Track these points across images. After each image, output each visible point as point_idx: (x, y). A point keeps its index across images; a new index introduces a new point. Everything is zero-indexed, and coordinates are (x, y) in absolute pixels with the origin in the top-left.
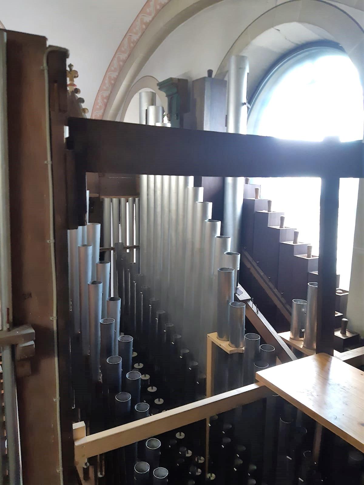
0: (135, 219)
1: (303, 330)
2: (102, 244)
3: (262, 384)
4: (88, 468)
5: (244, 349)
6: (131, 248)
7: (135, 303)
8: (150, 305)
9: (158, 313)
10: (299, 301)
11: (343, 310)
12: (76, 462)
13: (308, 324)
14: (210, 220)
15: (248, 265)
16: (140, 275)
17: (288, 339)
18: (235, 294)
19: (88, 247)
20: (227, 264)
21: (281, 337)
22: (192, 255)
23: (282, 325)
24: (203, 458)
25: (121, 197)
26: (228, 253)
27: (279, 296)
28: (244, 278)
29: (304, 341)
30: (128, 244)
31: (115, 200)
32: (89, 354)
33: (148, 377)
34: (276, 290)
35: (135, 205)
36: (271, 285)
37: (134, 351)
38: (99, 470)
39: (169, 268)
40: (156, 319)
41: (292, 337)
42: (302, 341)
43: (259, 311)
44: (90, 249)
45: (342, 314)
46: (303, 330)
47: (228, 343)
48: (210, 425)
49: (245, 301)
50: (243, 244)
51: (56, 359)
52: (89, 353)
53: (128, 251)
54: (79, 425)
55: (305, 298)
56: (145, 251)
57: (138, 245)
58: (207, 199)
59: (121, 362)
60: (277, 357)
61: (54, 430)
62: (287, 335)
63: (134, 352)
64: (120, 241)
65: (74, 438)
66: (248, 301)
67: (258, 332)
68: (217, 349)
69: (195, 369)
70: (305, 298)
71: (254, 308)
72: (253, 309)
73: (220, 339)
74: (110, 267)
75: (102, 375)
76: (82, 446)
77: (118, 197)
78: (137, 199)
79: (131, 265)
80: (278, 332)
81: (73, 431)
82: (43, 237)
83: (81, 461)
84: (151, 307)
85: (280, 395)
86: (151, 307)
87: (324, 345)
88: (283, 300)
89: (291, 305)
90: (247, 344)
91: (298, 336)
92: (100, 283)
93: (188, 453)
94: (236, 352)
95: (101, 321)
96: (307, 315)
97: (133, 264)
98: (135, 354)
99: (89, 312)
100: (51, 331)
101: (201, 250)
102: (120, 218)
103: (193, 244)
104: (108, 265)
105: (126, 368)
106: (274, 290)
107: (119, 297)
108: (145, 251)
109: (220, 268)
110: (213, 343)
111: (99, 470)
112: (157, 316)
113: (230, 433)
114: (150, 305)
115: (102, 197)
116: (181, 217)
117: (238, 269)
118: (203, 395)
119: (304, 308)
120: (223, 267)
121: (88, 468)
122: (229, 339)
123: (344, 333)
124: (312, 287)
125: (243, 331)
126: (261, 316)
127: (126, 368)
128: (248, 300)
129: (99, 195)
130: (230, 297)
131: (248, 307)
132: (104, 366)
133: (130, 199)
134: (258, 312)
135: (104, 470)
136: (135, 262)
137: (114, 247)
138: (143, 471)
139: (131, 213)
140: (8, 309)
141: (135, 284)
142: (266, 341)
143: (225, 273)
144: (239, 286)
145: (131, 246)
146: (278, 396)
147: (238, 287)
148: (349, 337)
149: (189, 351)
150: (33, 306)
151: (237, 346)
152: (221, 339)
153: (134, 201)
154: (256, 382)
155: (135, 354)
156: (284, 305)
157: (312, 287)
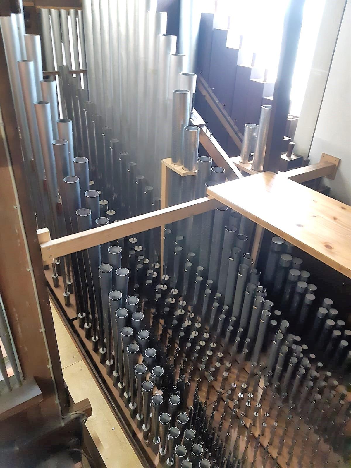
0: (80, 37)
1: (252, 154)
2: (44, 67)
4: (57, 278)
5: (196, 171)
6: (78, 72)
8: (103, 134)
10: (251, 125)
11: (291, 135)
12: (44, 262)
13: (257, 148)
14: (164, 35)
15: (204, 93)
16: (90, 102)
17: (238, 163)
18: (189, 119)
19: (29, 62)
20: (182, 86)
22: (146, 77)
23: (233, 151)
24: (156, 273)
25: (60, 8)
26: (184, 74)
27: (232, 123)
28: (199, 103)
29: (252, 164)
30: (74, 68)
31: (54, 12)
32: (46, 179)
33: (106, 202)
34: (230, 118)
35: (78, 20)
36: (225, 112)
37: (90, 180)
38: (67, 278)
40: (110, 147)
41: (242, 161)
42: (250, 164)
43: (212, 136)
44: (31, 64)
45: (290, 139)
46: (252, 154)
48: (164, 238)
49: (200, 126)
50: (200, 65)
51: (10, 168)
52: (45, 178)
54: (43, 231)
55: (257, 122)
56: (288, 297)
57: (84, 69)
58: (160, 9)
60: (226, 178)
61: (19, 236)
62: (238, 159)
63: (91, 181)
64: (65, 64)
66: (202, 126)
67: (209, 156)
68: (171, 173)
69: (150, 193)
70: (257, 122)
71: (208, 133)
72: (206, 134)
73: (174, 163)
74: (55, 85)
75: (60, 198)
76: (48, 248)
77: (58, 7)
78: (79, 11)
79: (79, 91)
80: (230, 156)
81: (38, 235)
83: (49, 259)
84: (104, 136)
86: (104, 136)
87: (272, 164)
88: (235, 127)
89: (242, 131)
91: (247, 161)
92: (47, 103)
93: (145, 261)
95: (53, 142)
96: (257, 139)
97: (81, 90)
98: (92, 183)
99: (40, 133)
101: (155, 72)
102: (62, 36)
103: (146, 64)
104: (53, 84)
106: (228, 118)
107: (69, 118)
108: (94, 76)
109: (175, 90)
111: (67, 278)
113: (182, 243)
114: (103, 134)
115: (39, 7)
116: (131, 32)
117: (194, 92)
118: (158, 207)
119: (256, 133)
121: (57, 278)
122: (182, 163)
123: (289, 156)
124: (266, 109)
125: (197, 155)
126: (214, 140)
128: (203, 125)
129: (34, 4)
131: (201, 131)
132: (62, 185)
133: (72, 11)
134: (211, 137)
135: (71, 277)
136: (83, 88)
137: (59, 71)
139: (74, 26)
141: (86, 112)
143: (180, 95)
144: (194, 111)
145: (77, 70)
148: (294, 159)
149: (144, 177)
151: (190, 169)
154: (207, 196)
155: (92, 183)
156: (236, 134)
157: (266, 109)
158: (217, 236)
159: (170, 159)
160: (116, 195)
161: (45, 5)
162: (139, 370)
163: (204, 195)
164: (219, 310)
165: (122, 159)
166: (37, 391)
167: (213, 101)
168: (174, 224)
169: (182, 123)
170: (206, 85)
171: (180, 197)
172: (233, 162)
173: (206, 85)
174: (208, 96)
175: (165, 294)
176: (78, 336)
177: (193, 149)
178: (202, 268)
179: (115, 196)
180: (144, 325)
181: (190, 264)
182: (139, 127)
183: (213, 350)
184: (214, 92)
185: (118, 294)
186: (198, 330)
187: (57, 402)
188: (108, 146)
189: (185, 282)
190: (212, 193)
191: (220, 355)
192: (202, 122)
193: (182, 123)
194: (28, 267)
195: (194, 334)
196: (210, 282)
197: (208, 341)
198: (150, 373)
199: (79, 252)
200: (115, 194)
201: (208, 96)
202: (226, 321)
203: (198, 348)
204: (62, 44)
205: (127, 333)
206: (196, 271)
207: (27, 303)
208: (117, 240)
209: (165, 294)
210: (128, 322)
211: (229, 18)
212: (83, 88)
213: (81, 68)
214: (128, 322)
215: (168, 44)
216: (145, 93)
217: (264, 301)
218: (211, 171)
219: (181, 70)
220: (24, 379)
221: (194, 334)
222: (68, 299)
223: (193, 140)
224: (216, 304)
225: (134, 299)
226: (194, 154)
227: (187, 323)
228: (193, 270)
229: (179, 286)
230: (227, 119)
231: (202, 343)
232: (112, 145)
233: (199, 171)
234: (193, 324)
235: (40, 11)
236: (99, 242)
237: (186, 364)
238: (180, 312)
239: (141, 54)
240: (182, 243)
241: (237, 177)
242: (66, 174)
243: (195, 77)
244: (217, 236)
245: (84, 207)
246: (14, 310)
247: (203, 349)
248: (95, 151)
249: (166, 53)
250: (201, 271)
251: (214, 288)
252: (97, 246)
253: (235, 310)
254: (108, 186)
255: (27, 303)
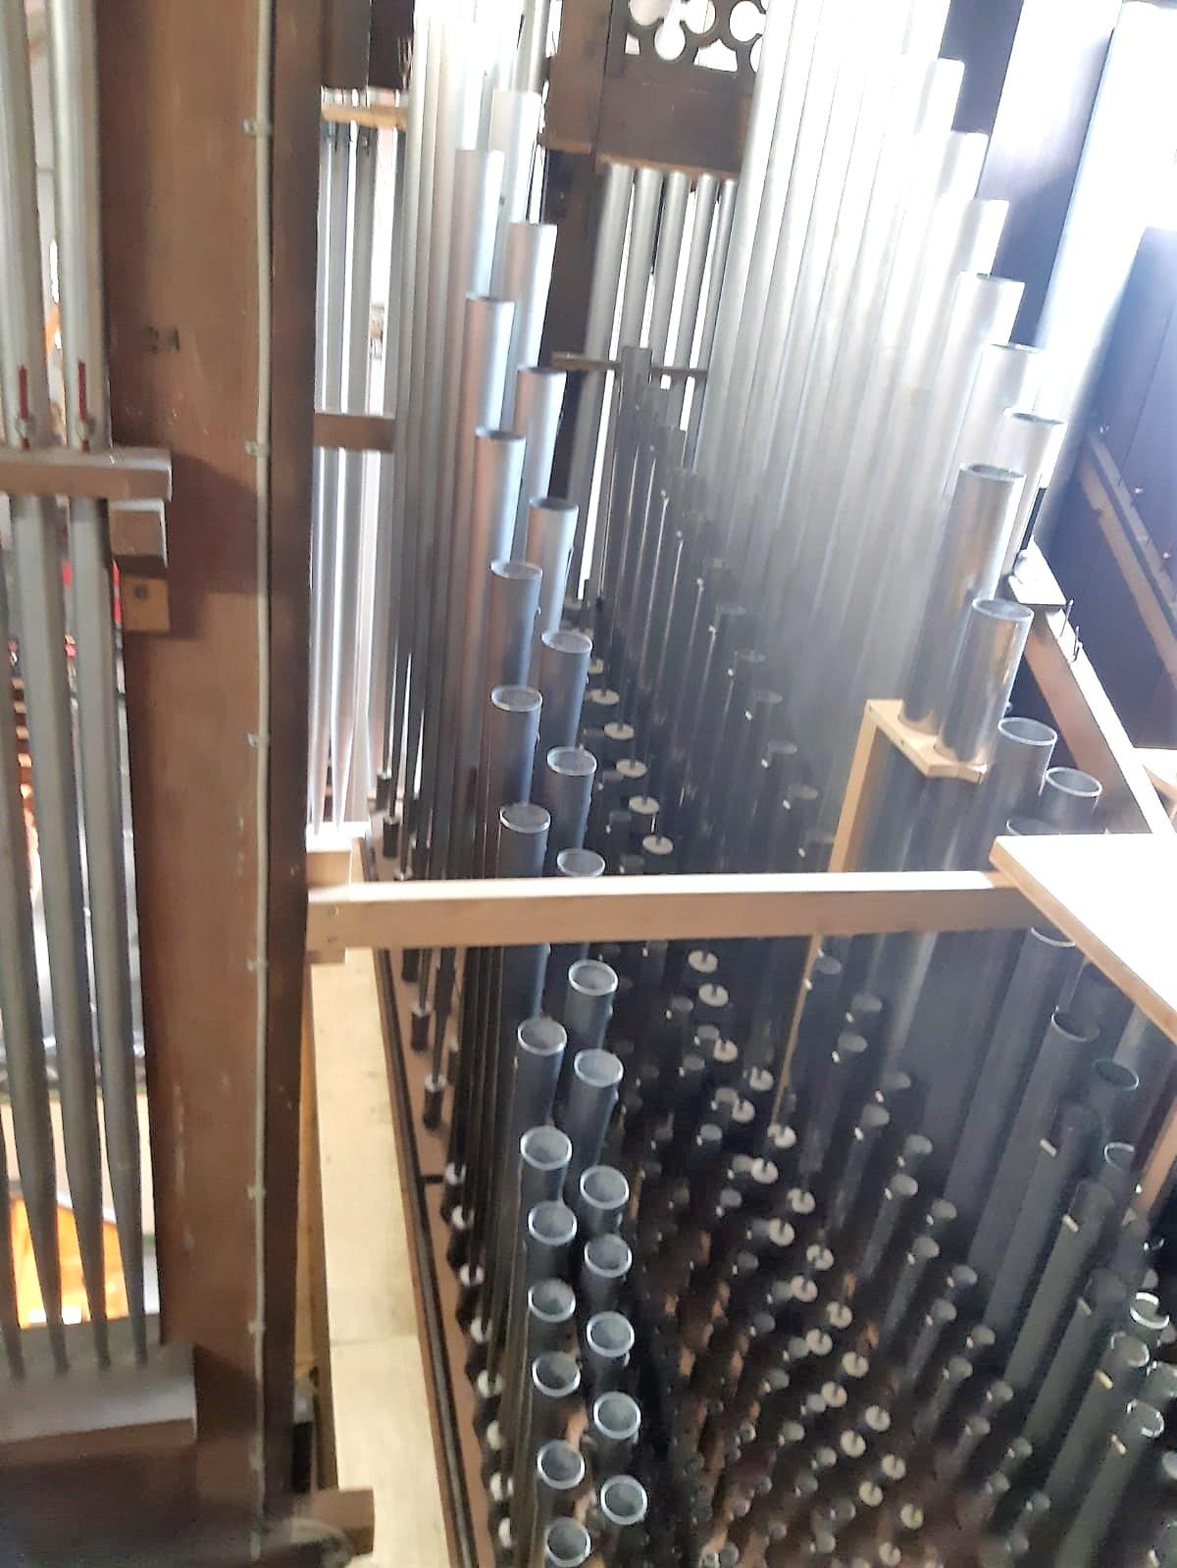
3: (1005, 880)
6: (679, 375)
7: (655, 575)
9: (719, 610)
15: (1098, 499)
20: (1005, 455)
21: (1146, 770)
22: (885, 415)
30: (669, 362)
31: (649, 176)
39: (793, 455)
47: (933, 740)
49: (1041, 611)
51: (261, 603)
53: (666, 382)
56: (724, 393)
57: (703, 367)
59: (536, 709)
61: (247, 841)
64: (644, 343)
65: (309, 880)
76: (330, 908)
78: (729, 184)
82: (229, 108)
85: (1080, 946)
90: (1003, 751)
92: (519, 438)
94: (954, 774)
100: (247, 494)
101: (922, 398)
105: (552, 735)
108: (724, 393)
110: (880, 735)
112: (769, 754)
118: (817, 862)
120: (988, 463)
125: (1001, 708)
126: (1084, 672)
127: (552, 735)
128: (1054, 608)
130: (980, 581)
131: (1040, 626)
136: (684, 426)
138: (543, 1046)
140: (82, 367)
142: (1078, 762)
144: (1034, 554)
146: (1065, 945)
147: (1024, 553)
149: (795, 750)
150: (185, 383)
152: (913, 724)
153: (717, 192)
154: (989, 868)
158: (1011, 1040)
159: (896, 707)
160: (691, 789)
161: (623, 154)
162: (554, 1468)
163: (974, 858)
164: (950, 1338)
165: (737, 672)
166: (179, 1404)
167: (1125, 533)
168: (862, 943)
169: (970, 583)
170: (1113, 474)
171: (906, 849)
172: (1144, 768)
173: (1113, 474)
174: (1109, 513)
175: (761, 1201)
176: (429, 1243)
177: (990, 685)
178: (928, 1148)
179: (688, 792)
180: (625, 1296)
181: (880, 1117)
182: (824, 575)
183: (886, 1485)
184: (1137, 502)
185: (563, 1149)
186: (849, 1384)
187: (257, 1463)
188: (707, 618)
189: (846, 1173)
190: (1011, 863)
191: (910, 1517)
192: (1053, 594)
193: (970, 583)
194: (254, 958)
195: (830, 1396)
196: (945, 1210)
197: (876, 1444)
198: (593, 1497)
199: (485, 949)
200: (689, 787)
201: (1109, 513)
202: (968, 1395)
203: (829, 1457)
204: (651, 278)
205: (553, 1308)
206: (900, 1148)
207: (225, 1081)
208: (642, 944)
209: (761, 1201)
210: (568, 1265)
211: (904, 52)
212: (684, 426)
213: (693, 365)
214: (568, 1265)
215: (986, 308)
216: (874, 465)
217: (1149, 1364)
218: (1043, 782)
219: (1013, 398)
220: (163, 1341)
221: (830, 1396)
222: (434, 1099)
223: (998, 654)
224: (947, 1311)
225: (613, 1188)
226: (991, 703)
227: (815, 1343)
228: (887, 1142)
229: (820, 1188)
230: (1167, 607)
231: (852, 1444)
232: (717, 619)
233: (994, 771)
234: (835, 1355)
235: (607, 169)
236: (545, 935)
237: (763, 1505)
238: (801, 1289)
239: (889, 336)
240: (877, 1029)
241: (1140, 825)
242: (510, 677)
243: (549, 234)
244: (1011, 1040)
245: (539, 798)
246: (177, 1090)
247: (847, 1472)
248: (664, 630)
249: (972, 341)
250: (919, 1156)
251: (956, 1244)
252: (535, 949)
253: (1022, 1359)
254: (676, 754)
255: (225, 1081)
